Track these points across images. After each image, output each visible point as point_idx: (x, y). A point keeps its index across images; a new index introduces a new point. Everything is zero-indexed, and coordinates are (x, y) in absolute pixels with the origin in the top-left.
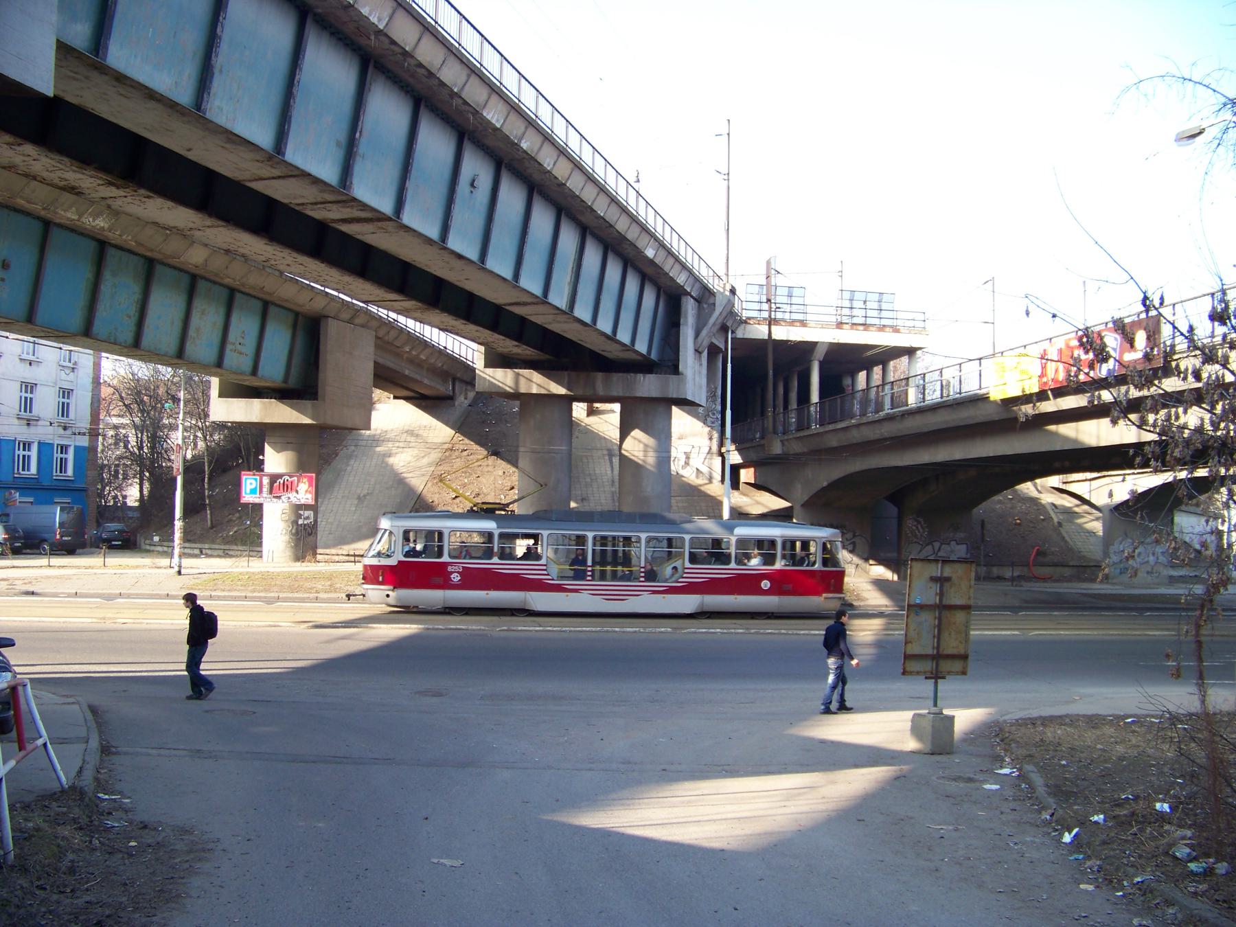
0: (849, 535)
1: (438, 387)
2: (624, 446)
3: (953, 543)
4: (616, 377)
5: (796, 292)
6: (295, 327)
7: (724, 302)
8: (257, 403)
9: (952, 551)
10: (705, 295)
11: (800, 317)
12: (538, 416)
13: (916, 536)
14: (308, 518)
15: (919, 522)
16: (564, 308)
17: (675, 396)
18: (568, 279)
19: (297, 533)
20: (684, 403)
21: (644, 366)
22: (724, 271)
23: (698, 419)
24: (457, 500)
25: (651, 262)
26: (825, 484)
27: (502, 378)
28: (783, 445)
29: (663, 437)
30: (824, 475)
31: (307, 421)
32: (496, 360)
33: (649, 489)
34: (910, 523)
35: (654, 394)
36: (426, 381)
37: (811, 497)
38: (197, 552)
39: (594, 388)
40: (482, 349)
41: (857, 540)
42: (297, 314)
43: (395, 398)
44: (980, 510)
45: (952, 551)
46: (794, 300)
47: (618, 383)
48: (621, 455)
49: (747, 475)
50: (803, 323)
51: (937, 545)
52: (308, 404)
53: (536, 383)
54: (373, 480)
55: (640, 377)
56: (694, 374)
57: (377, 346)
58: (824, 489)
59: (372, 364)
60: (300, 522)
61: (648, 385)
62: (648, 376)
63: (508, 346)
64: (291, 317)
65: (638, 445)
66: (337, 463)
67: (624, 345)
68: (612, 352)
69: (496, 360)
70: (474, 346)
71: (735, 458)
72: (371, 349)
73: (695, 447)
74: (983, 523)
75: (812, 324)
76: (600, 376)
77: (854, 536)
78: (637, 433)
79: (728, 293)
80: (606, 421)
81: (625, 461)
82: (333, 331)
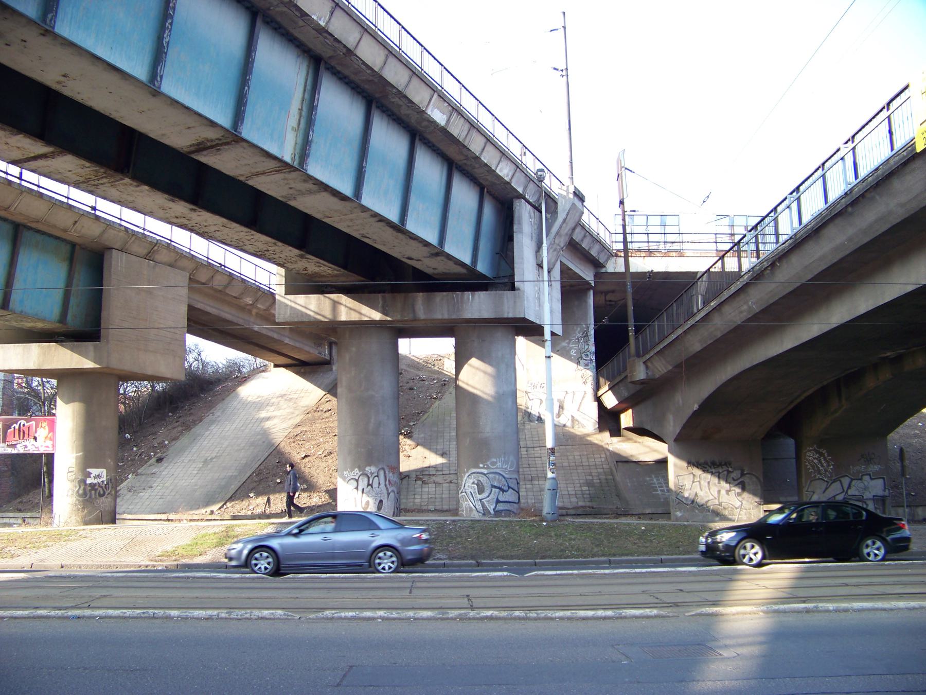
0: (736, 474)
1: (312, 351)
2: (461, 376)
3: (866, 478)
4: (439, 297)
5: (669, 220)
6: (71, 260)
7: (568, 208)
8: (35, 348)
9: (866, 488)
10: (547, 203)
11: (676, 246)
12: (354, 349)
13: (819, 472)
14: (98, 477)
15: (821, 454)
16: (287, 158)
17: (511, 316)
18: (293, 121)
19: (85, 494)
20: (533, 331)
21: (469, 281)
22: (568, 174)
23: (571, 360)
24: (307, 459)
25: (444, 131)
26: (696, 407)
27: (313, 306)
28: (647, 367)
29: (506, 372)
30: (690, 398)
31: (89, 364)
32: (299, 284)
33: (488, 429)
34: (810, 456)
35: (486, 315)
36: (287, 341)
37: (684, 428)
38: (20, 521)
39: (414, 311)
40: (282, 271)
41: (746, 479)
42: (73, 245)
43: (276, 366)
44: (898, 437)
45: (866, 488)
46: (668, 230)
47: (441, 307)
48: (458, 387)
49: (627, 419)
50: (680, 254)
51: (846, 481)
52: (90, 345)
53: (350, 309)
54: (226, 443)
55: (468, 295)
56: (540, 298)
57: (191, 289)
58: (695, 413)
59: (184, 309)
60: (89, 481)
61: (478, 305)
62: (477, 293)
63: (313, 265)
64: (65, 249)
65: (476, 377)
66: (197, 429)
67: (427, 244)
68: (429, 265)
69: (299, 284)
70: (274, 268)
71: (610, 401)
72: (184, 292)
73: (557, 388)
74: (901, 450)
75: (688, 253)
76: (420, 297)
77: (742, 475)
78: (474, 361)
79: (571, 196)
80: (429, 351)
81: (462, 395)
82: (117, 264)
